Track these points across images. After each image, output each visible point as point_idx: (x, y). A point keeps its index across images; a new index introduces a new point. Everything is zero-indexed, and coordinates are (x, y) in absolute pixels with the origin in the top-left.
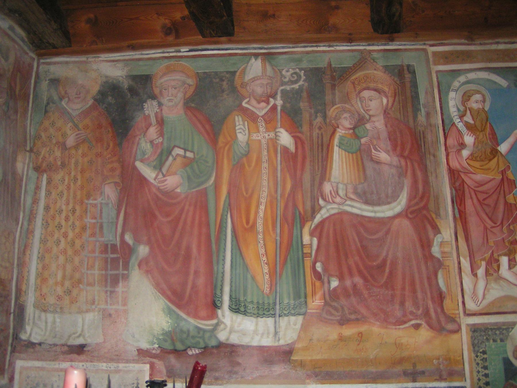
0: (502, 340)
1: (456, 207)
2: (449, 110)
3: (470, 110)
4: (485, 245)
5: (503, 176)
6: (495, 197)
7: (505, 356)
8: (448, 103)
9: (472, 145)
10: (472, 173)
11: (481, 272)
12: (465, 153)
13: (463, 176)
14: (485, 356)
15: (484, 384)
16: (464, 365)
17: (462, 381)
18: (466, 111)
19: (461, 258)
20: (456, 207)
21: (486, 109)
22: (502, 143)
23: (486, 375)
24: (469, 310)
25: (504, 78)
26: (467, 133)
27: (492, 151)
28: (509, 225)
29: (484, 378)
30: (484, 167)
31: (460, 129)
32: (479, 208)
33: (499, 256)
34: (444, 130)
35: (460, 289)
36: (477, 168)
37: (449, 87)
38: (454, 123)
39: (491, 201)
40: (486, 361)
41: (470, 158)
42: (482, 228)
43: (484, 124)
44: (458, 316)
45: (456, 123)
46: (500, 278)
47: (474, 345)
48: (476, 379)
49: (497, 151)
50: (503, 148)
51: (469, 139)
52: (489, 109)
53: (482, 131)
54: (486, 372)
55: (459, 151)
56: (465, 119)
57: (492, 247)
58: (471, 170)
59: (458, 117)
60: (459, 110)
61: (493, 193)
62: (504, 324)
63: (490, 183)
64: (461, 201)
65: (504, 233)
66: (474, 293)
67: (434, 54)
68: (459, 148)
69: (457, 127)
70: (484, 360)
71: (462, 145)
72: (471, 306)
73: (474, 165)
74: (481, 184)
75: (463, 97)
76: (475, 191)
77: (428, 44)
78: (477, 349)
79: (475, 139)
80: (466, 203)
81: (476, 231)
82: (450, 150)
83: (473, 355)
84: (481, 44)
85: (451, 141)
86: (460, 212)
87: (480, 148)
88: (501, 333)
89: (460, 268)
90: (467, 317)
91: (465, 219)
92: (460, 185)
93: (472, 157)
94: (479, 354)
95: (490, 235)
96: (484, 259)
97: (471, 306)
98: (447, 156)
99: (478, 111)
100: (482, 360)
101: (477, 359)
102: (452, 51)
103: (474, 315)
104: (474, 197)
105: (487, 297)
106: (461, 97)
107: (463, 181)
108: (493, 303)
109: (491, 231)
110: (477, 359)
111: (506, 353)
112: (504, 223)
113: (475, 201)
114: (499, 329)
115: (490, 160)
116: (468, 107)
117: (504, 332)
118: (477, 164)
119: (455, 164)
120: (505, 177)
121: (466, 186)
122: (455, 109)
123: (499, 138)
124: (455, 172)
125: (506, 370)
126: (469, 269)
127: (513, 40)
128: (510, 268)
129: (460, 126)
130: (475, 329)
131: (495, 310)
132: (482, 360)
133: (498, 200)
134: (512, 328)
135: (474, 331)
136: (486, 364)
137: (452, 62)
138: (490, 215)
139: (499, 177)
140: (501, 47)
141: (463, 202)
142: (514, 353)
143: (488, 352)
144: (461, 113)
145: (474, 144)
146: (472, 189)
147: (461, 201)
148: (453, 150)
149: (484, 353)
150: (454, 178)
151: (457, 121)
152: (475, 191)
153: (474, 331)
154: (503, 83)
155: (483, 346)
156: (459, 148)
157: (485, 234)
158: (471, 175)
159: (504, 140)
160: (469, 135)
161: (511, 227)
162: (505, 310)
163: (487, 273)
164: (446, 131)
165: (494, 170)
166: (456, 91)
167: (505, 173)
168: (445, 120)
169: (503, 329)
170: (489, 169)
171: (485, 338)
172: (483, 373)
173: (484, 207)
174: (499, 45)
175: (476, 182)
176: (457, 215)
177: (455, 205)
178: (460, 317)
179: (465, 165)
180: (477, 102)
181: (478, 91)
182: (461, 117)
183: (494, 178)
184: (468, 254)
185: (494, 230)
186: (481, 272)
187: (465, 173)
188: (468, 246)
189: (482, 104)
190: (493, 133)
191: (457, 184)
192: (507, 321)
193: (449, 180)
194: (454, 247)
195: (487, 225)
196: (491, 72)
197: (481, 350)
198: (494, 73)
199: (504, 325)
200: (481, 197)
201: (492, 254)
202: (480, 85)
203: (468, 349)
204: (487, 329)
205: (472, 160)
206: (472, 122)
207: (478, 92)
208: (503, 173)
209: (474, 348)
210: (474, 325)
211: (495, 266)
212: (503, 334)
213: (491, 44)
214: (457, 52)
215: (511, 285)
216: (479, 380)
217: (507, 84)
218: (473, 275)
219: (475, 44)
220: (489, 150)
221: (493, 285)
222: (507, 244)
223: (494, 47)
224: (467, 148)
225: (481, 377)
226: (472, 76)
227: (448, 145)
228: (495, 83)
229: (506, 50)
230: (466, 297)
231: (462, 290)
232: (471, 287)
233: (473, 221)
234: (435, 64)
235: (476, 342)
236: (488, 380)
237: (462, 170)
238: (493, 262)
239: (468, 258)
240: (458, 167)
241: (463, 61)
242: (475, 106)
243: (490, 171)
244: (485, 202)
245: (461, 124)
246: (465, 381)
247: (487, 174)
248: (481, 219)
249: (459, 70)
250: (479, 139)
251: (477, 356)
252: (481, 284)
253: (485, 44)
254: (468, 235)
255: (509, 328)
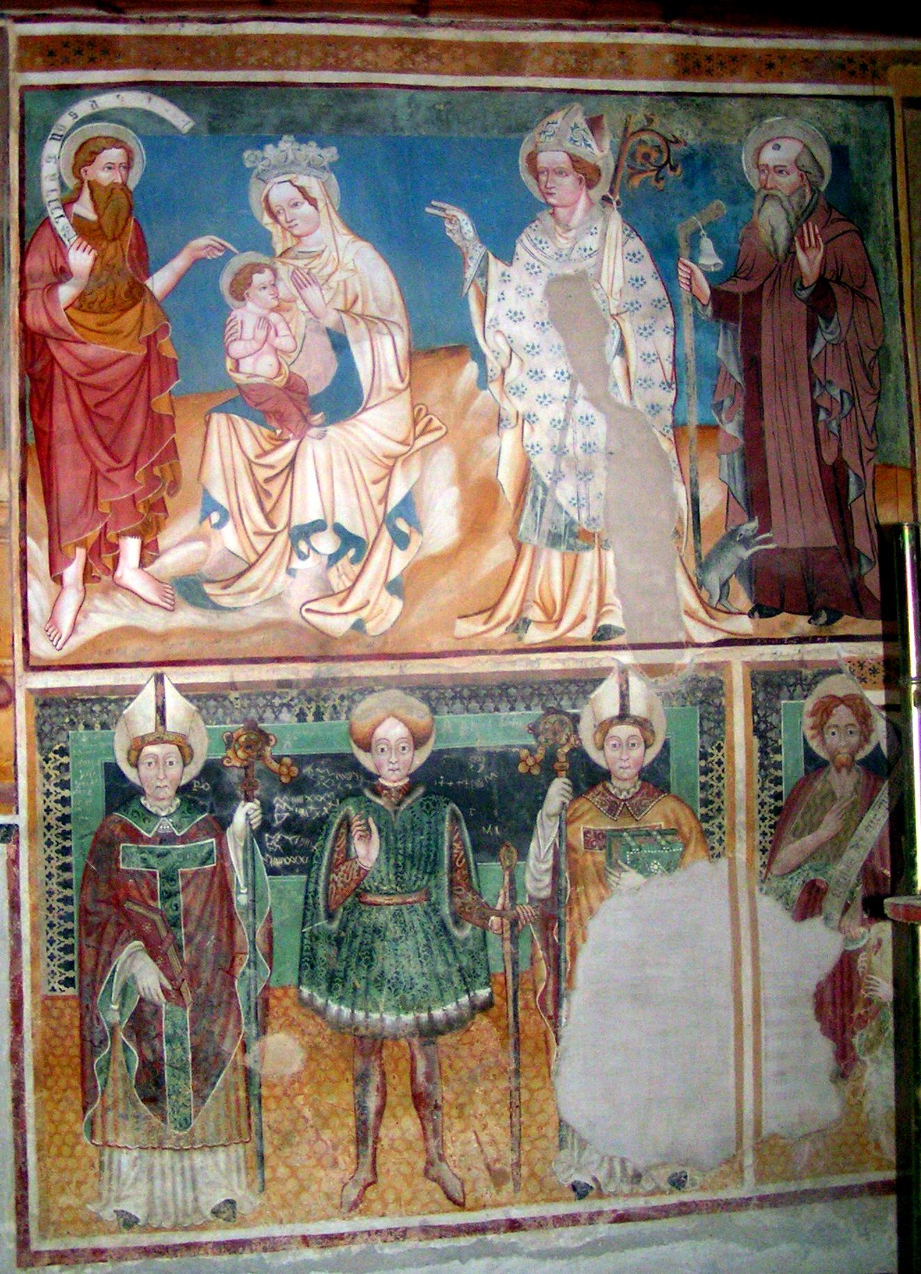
0: (104, 726)
1: (29, 422)
2: (40, 188)
3: (89, 186)
4: (90, 511)
5: (149, 350)
6: (124, 398)
7: (109, 759)
8: (39, 170)
9: (87, 271)
10: (77, 341)
11: (72, 573)
12: (66, 293)
13: (52, 345)
14: (65, 760)
15: (58, 819)
16: (16, 779)
17: (9, 812)
18: (80, 190)
19: (30, 540)
20: (29, 422)
21: (132, 185)
22: (157, 271)
23: (65, 801)
24: (39, 658)
25: (186, 110)
26: (76, 245)
27: (131, 288)
28: (152, 465)
29: (59, 806)
30: (109, 328)
31: (61, 234)
32: (84, 425)
33: (118, 536)
34: (22, 235)
35: (19, 611)
36: (91, 330)
37: (48, 128)
38: (48, 218)
39: (113, 410)
40: (67, 769)
41: (77, 304)
42: (85, 472)
43: (121, 223)
44: (9, 671)
45: (52, 219)
46: (119, 587)
47: (42, 735)
48: (41, 808)
49: (143, 290)
50: (159, 282)
51: (80, 259)
52: (138, 187)
53: (114, 239)
54: (66, 793)
55: (52, 287)
56: (77, 208)
57: (104, 515)
58: (76, 334)
59: (57, 204)
60: (63, 185)
61: (121, 390)
62: (113, 689)
63: (119, 366)
64: (42, 406)
65: (136, 484)
66: (53, 619)
67: (24, 41)
68: (54, 280)
69: (53, 230)
70: (63, 768)
71: (63, 273)
72: (42, 648)
73: (85, 323)
74: (92, 368)
75: (76, 154)
76: (78, 383)
77: (10, 17)
78: (47, 743)
79: (96, 259)
80: (55, 414)
81: (70, 479)
82: (30, 285)
83: (39, 757)
84: (142, 21)
85: (36, 263)
86: (37, 430)
87: (103, 279)
88: (105, 710)
89: (24, 564)
90: (31, 674)
91: (50, 448)
92: (44, 369)
93: (81, 302)
94: (51, 755)
95: (103, 489)
96: (82, 544)
97: (42, 648)
98: (23, 298)
99: (112, 189)
100: (58, 768)
101: (46, 766)
102: (68, 36)
103: (47, 668)
104: (75, 397)
105: (80, 628)
106: (73, 153)
107: (53, 359)
108: (93, 643)
109: (109, 480)
110: (46, 766)
111: (113, 754)
112: (140, 460)
113: (77, 406)
114: (100, 700)
115: (124, 311)
116: (86, 179)
117: (112, 707)
118: (91, 320)
119: (38, 319)
120: (153, 353)
121: (57, 371)
122: (55, 185)
123: (152, 258)
124: (37, 337)
125: (109, 791)
126: (46, 566)
127: (220, 15)
128: (142, 564)
129: (62, 225)
130: (46, 701)
131: (97, 659)
132: (58, 768)
133: (131, 404)
134: (131, 700)
135: (44, 705)
136: (66, 778)
137: (65, 65)
138: (108, 441)
139: (140, 352)
140: (190, 30)
141: (47, 413)
142: (129, 753)
143: (72, 752)
144: (66, 194)
145: (92, 271)
146: (71, 377)
147: (42, 406)
148: (36, 285)
149: (63, 752)
150: (33, 352)
151: (55, 213)
152: (78, 383)
153: (44, 705)
154: (180, 120)
155: (62, 737)
156: (54, 280)
157: (92, 488)
158: (73, 347)
159: (162, 264)
160: (82, 248)
161: (156, 471)
162: (121, 660)
163: (87, 575)
164: (28, 239)
165: (129, 335)
166: (63, 138)
167: (156, 342)
168: (27, 212)
169: (111, 702)
170: (117, 332)
171: (67, 720)
172: (59, 797)
173: (97, 421)
174: (187, 25)
175: (84, 364)
176: (31, 441)
177: (28, 417)
178: (14, 674)
179: (62, 320)
180: (110, 167)
181: (118, 140)
182: (66, 205)
183: (129, 355)
184: (45, 531)
185: (114, 476)
186: (72, 573)
187: (57, 339)
188: (49, 514)
189: (124, 172)
190: (141, 245)
191: (38, 366)
192: (121, 683)
193: (21, 356)
194: (16, 514)
195: (98, 464)
196: (154, 93)
197: (57, 748)
198: (162, 96)
199: (113, 693)
200: (92, 398)
201: (104, 531)
202: (125, 124)
203: (29, 745)
204: (71, 700)
205: (79, 308)
206: (92, 216)
207: (116, 143)
208: (151, 341)
209: (41, 741)
210: (45, 691)
211: (107, 559)
212: (108, 712)
213: (168, 20)
214: (78, 38)
215: (142, 603)
216: (48, 810)
217: (191, 124)
218: (54, 579)
219: (126, 21)
220: (123, 287)
221: (98, 602)
222: (141, 510)
223: (173, 29)
224: (72, 280)
225: (53, 805)
226: (107, 101)
227: (27, 272)
228: (162, 121)
229: (202, 39)
230: (31, 628)
231: (25, 612)
232: (46, 605)
233: (66, 453)
234: (23, 67)
235: (46, 728)
236: (67, 810)
237: (53, 334)
238: (103, 549)
239: (46, 542)
240: (47, 326)
241: (92, 64)
242: (103, 175)
243: (121, 336)
244: (100, 411)
245: (64, 221)
246: (17, 812)
247: (113, 344)
248: (87, 452)
249: (79, 86)
250: (107, 257)
251: (47, 760)
252: (70, 600)
253: (153, 21)
254: (51, 485)
255: (123, 700)
